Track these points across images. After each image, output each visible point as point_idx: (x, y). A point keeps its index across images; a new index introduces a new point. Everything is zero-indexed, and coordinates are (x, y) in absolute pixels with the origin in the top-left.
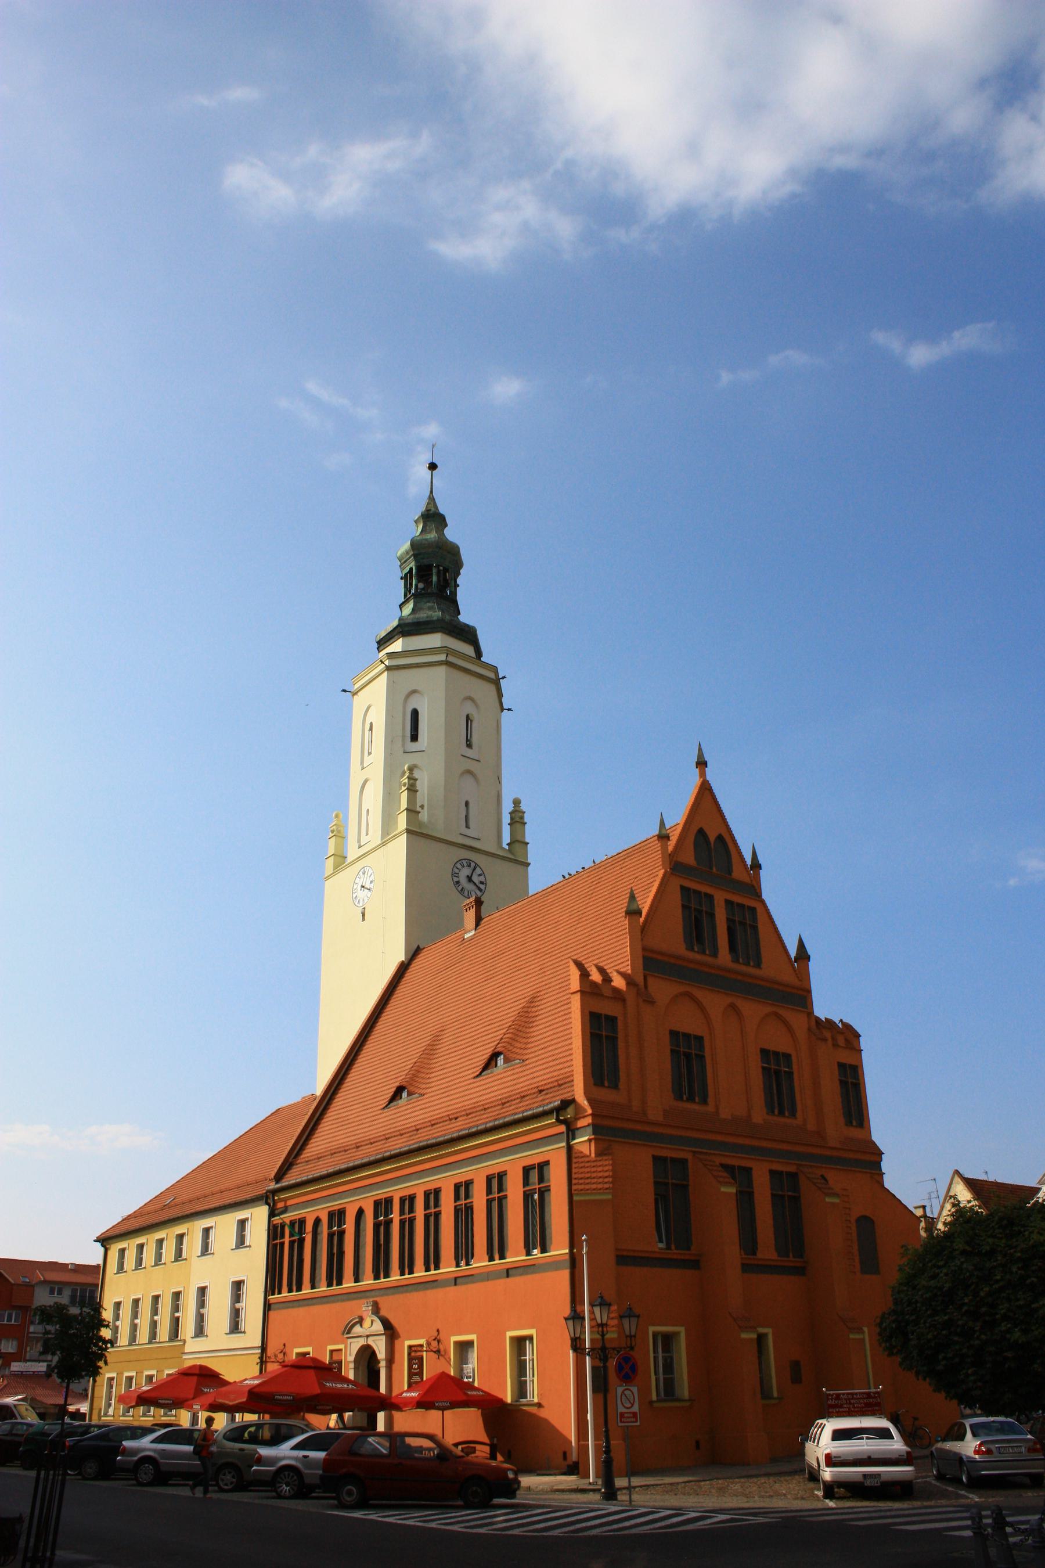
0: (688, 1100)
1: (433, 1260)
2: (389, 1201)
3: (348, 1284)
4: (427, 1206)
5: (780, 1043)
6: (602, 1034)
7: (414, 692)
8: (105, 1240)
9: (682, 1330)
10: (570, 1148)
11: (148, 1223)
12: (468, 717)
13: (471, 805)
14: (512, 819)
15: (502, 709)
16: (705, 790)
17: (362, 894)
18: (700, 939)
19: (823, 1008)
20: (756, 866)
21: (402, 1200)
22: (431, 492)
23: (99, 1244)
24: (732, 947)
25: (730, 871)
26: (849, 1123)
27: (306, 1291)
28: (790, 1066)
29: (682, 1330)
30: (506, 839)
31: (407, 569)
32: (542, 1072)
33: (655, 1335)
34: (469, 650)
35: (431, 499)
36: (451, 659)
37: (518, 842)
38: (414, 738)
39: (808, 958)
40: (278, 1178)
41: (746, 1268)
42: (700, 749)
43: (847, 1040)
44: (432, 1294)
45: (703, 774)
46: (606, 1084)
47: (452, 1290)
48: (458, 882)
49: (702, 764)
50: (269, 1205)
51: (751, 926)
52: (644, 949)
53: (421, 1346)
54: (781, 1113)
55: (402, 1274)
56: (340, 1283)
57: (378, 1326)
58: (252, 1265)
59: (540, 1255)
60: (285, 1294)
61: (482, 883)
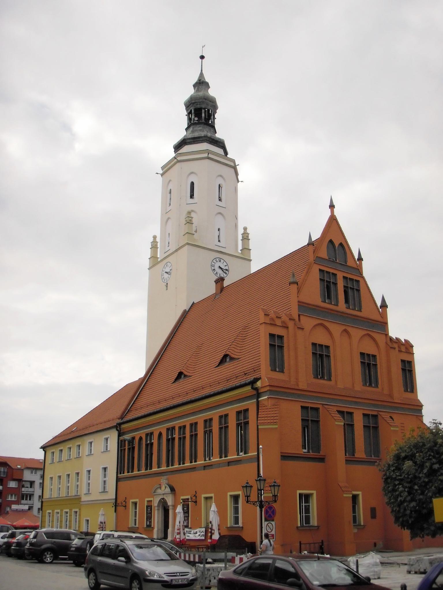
0: (321, 378)
1: (194, 457)
2: (173, 428)
3: (155, 469)
4: (191, 431)
5: (370, 349)
6: (276, 344)
7: (192, 173)
8: (44, 448)
9: (314, 492)
10: (258, 402)
11: (62, 440)
12: (219, 185)
13: (221, 230)
14: (243, 237)
15: (238, 181)
16: (333, 221)
17: (166, 276)
18: (329, 297)
19: (394, 332)
20: (360, 259)
21: (180, 428)
22: (202, 71)
23: (42, 450)
24: (347, 301)
25: (346, 262)
26: (406, 390)
27: (136, 472)
28: (375, 361)
29: (314, 492)
30: (240, 247)
31: (189, 111)
32: (247, 365)
33: (301, 495)
34: (221, 151)
35: (201, 74)
36: (210, 156)
37: (246, 249)
38: (192, 196)
39: (387, 307)
40: (122, 417)
41: (348, 461)
42: (331, 200)
43: (406, 348)
44: (194, 475)
45: (332, 212)
46: (277, 370)
47: (203, 472)
48: (214, 270)
49: (332, 206)
50: (117, 430)
51: (356, 289)
52: (299, 302)
53: (188, 499)
54: (370, 385)
55: (180, 464)
56: (151, 468)
57: (168, 490)
58: (111, 460)
59: (244, 455)
60: (126, 474)
61: (227, 270)
